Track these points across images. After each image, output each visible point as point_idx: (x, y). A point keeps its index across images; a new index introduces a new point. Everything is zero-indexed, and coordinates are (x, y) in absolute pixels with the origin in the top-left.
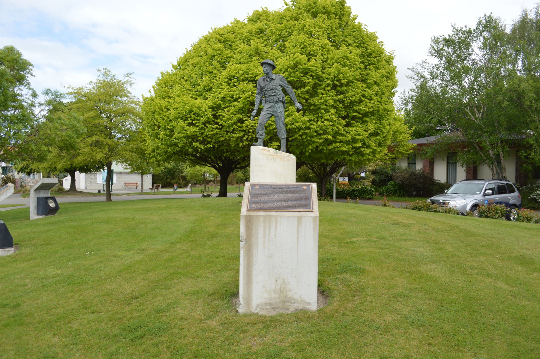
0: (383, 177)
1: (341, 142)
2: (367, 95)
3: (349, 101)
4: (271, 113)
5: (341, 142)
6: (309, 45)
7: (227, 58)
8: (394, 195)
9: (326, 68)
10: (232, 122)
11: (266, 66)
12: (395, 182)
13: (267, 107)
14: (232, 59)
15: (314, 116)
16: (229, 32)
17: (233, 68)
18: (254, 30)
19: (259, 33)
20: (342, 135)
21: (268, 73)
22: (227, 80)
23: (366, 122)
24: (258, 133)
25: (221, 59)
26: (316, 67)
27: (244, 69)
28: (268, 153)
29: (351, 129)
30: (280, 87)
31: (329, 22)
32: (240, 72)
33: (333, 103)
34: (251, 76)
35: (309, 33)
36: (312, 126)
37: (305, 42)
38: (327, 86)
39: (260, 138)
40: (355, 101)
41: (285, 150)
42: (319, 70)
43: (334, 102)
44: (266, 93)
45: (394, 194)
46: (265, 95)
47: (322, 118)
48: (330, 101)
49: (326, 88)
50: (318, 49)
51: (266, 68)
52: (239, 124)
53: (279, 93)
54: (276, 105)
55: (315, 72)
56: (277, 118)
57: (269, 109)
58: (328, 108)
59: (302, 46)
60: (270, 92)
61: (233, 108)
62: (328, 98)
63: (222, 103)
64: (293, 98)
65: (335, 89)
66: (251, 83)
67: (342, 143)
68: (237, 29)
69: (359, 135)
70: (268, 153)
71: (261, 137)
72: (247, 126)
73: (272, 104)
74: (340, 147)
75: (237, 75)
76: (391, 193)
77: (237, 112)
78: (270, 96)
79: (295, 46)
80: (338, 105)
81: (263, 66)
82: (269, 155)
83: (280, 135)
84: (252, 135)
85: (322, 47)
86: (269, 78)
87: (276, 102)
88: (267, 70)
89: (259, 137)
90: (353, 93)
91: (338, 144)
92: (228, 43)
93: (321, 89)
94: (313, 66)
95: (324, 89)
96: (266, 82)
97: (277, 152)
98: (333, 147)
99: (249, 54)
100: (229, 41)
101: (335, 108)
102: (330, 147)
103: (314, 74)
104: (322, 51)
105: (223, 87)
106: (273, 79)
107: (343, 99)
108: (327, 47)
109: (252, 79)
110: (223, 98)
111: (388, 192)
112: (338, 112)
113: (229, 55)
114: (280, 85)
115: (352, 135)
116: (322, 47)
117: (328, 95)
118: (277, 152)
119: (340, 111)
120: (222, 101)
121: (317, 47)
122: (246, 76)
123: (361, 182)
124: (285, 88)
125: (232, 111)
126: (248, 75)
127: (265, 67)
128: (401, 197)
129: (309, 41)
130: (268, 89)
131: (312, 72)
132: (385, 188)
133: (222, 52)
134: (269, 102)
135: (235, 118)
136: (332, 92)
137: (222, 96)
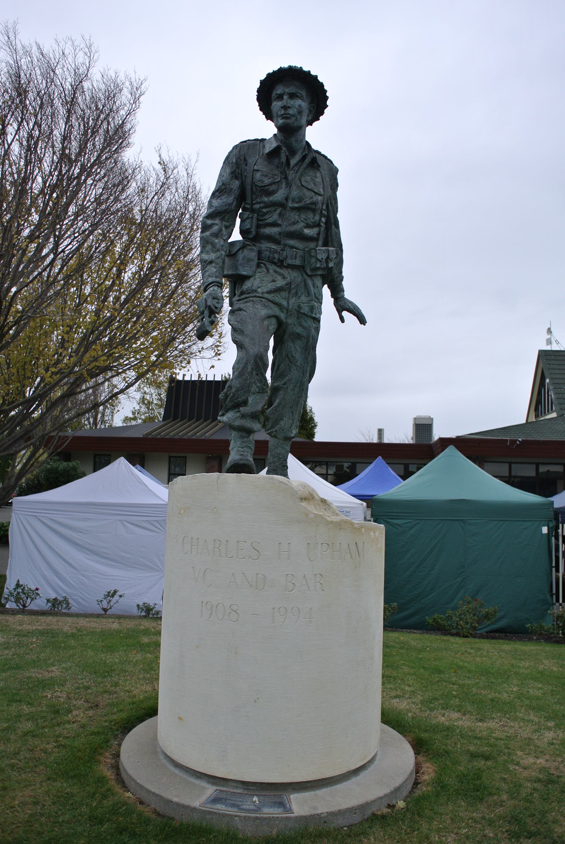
4: (282, 316)
13: (271, 286)
24: (245, 403)
51: (298, 102)
57: (277, 298)
60: (294, 216)
78: (292, 235)
130: (290, 204)
134: (280, 264)
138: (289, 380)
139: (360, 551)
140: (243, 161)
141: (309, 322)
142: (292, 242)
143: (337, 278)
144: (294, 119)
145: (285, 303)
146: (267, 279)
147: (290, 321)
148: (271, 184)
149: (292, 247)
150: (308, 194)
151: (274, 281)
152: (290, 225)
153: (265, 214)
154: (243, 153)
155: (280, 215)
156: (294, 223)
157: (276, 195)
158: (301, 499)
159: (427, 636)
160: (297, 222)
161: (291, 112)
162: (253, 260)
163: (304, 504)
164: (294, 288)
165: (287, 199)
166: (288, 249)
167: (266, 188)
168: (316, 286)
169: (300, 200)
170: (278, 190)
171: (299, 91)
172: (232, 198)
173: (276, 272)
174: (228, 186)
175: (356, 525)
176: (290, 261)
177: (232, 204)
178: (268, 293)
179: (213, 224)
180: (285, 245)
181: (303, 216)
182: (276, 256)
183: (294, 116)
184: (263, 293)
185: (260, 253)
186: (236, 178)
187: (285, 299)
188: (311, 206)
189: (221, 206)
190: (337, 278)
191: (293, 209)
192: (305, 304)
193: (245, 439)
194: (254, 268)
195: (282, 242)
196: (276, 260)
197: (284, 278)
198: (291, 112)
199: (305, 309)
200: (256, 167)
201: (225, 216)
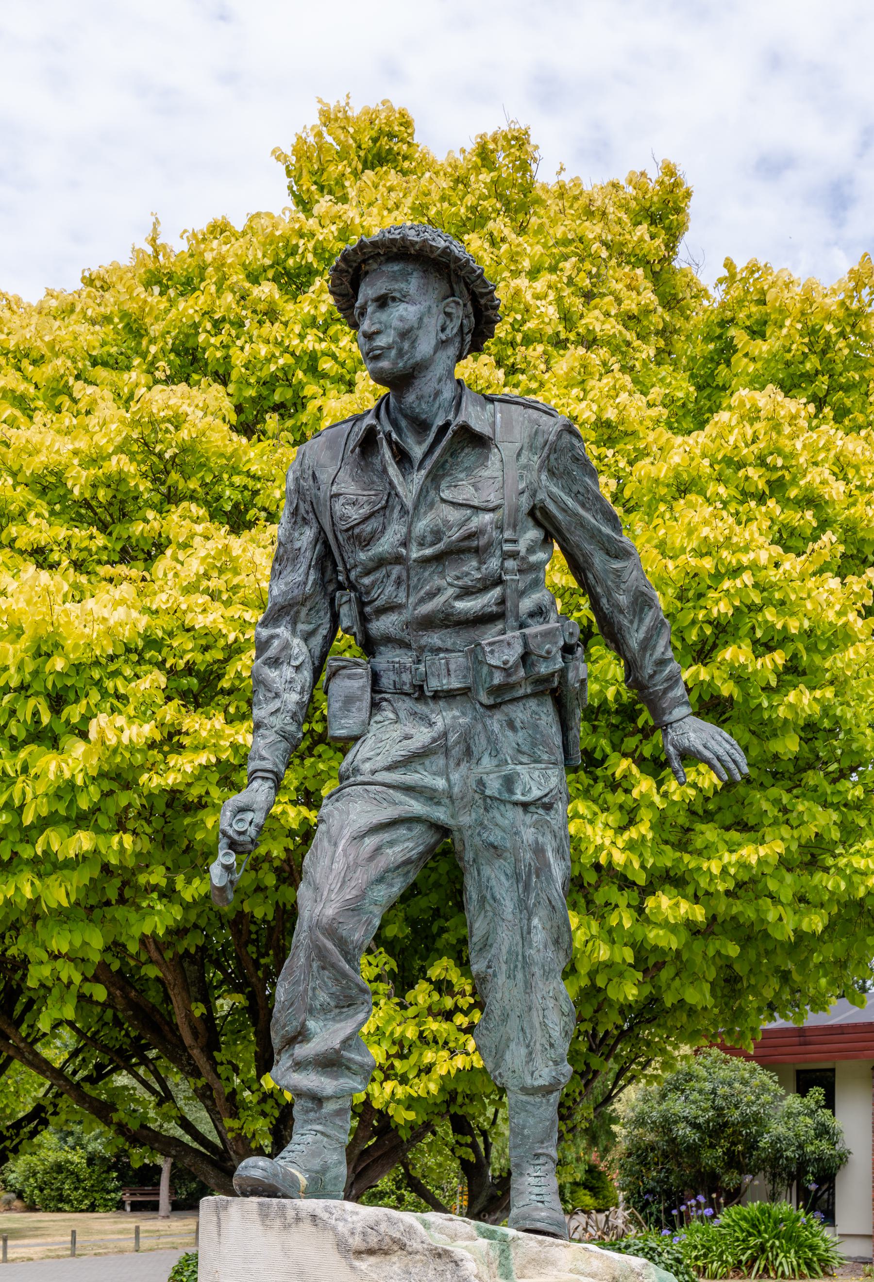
4: (440, 814)
13: (398, 752)
78: (428, 623)
89: (310, 1080)
96: (393, 471)
127: (383, 302)
130: (415, 554)
140: (311, 482)
142: (435, 639)
143: (651, 677)
144: (393, 352)
145: (440, 783)
146: (395, 734)
147: (465, 819)
148: (366, 519)
150: (454, 515)
151: (408, 737)
152: (422, 601)
157: (382, 540)
161: (381, 341)
164: (457, 743)
165: (405, 544)
167: (357, 531)
169: (437, 535)
170: (384, 528)
174: (289, 546)
176: (434, 684)
177: (305, 583)
178: (389, 768)
180: (422, 649)
183: (389, 348)
184: (374, 772)
188: (466, 544)
189: (284, 594)
191: (425, 561)
192: (492, 776)
194: (365, 714)
196: (407, 688)
197: (431, 724)
200: (335, 489)
201: (298, 612)
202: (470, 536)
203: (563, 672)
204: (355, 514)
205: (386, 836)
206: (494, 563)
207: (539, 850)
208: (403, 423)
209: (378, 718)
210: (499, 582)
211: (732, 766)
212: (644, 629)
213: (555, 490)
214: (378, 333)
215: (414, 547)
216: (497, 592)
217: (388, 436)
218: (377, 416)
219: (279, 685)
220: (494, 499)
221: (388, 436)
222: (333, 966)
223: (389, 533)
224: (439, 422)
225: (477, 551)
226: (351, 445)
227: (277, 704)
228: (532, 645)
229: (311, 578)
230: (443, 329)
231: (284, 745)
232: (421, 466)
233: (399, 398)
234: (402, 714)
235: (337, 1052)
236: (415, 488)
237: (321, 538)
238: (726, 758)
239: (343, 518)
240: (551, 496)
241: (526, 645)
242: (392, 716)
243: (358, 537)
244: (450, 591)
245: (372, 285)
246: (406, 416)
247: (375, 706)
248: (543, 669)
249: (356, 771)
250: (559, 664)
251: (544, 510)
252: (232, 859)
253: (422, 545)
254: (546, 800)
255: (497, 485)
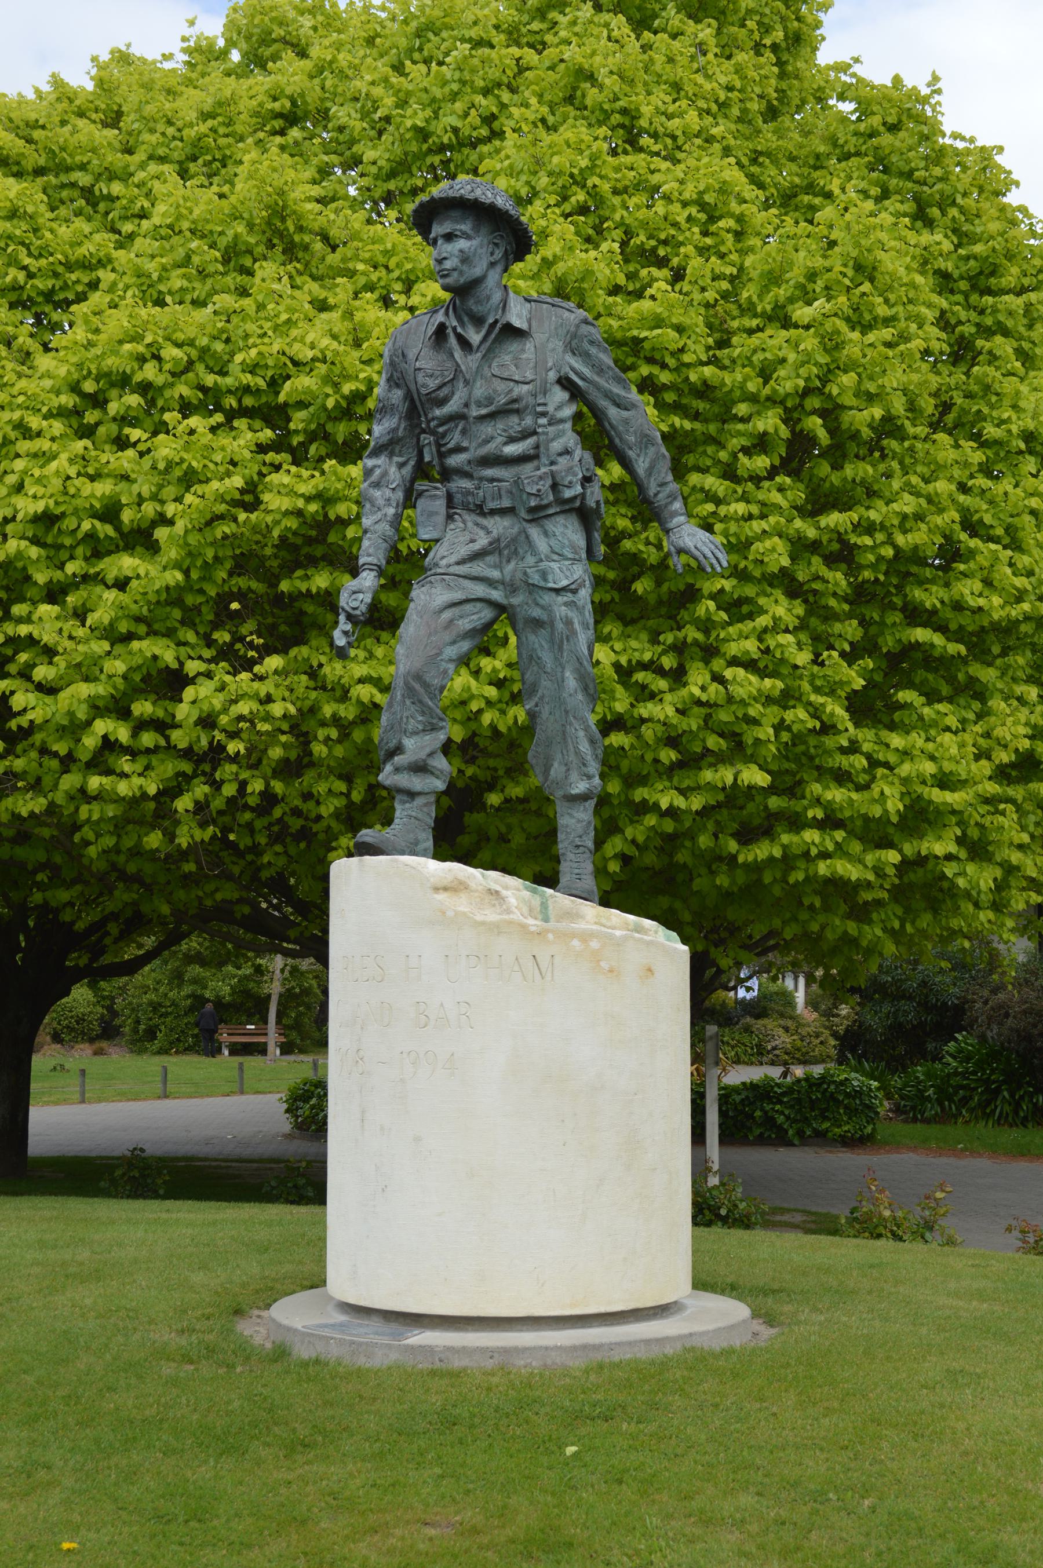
0: (910, 1013)
1: (830, 822)
2: (988, 519)
3: (888, 552)
4: (496, 595)
5: (830, 822)
6: (616, 192)
7: (69, 267)
8: (984, 1112)
9: (731, 333)
10: (100, 689)
11: (466, 227)
12: (982, 1038)
13: (464, 551)
14: (106, 276)
15: (654, 641)
16: (81, 114)
17: (117, 322)
18: (246, 105)
19: (278, 124)
20: (842, 777)
21: (477, 282)
22: (67, 400)
23: (978, 693)
24: (399, 750)
25: (31, 276)
26: (680, 329)
27: (191, 332)
28: (491, 915)
29: (897, 741)
30: (560, 395)
31: (728, 65)
32: (170, 352)
33: (785, 562)
34: (247, 379)
35: (616, 119)
36: (646, 710)
37: (591, 169)
38: (746, 451)
39: (412, 795)
40: (916, 557)
41: (589, 882)
42: (697, 350)
43: (793, 559)
44: (455, 439)
45: (984, 1105)
46: (442, 456)
47: (709, 652)
48: (768, 544)
49: (743, 459)
50: (681, 219)
51: (462, 244)
52: (143, 708)
53: (556, 446)
54: (534, 532)
55: (671, 362)
56: (538, 641)
57: (477, 568)
58: (750, 591)
59: (580, 196)
60: (487, 429)
61: (111, 595)
62: (757, 526)
63: (34, 552)
64: (652, 489)
65: (795, 474)
66: (241, 423)
67: (839, 835)
68: (130, 99)
69: (944, 782)
70: (491, 915)
71: (417, 783)
72: (207, 722)
73: (499, 526)
74: (825, 855)
75: (150, 372)
76: (964, 1101)
77: (138, 619)
78: (487, 461)
79: (530, 202)
80: (817, 578)
81: (438, 229)
82: (496, 929)
83: (557, 770)
84: (244, 775)
85: (703, 206)
86: (478, 321)
87: (537, 514)
88: (465, 259)
89: (404, 780)
90: (908, 504)
91: (811, 835)
92: (73, 185)
93: (704, 471)
94: (658, 322)
95: (730, 474)
96: (458, 354)
97: (544, 906)
98: (777, 853)
99: (223, 242)
100: (83, 167)
101: (794, 590)
102: (762, 851)
103: (665, 377)
104: (705, 233)
105: (44, 444)
106: (511, 332)
107: (853, 539)
108: (735, 207)
109: (248, 401)
110: (47, 520)
111: (951, 1101)
112: (814, 622)
113: (86, 249)
114: (565, 383)
115: (905, 781)
116: (703, 206)
117: (755, 509)
118: (544, 906)
119: (830, 616)
120: (35, 541)
121: (676, 207)
122: (210, 380)
123: (747, 1030)
124: (603, 403)
125: (100, 616)
126: (223, 373)
127: (449, 237)
128: (1024, 1122)
129: (617, 169)
130: (475, 412)
131: (650, 360)
132: (929, 1075)
133: (35, 231)
134: (480, 510)
135: (119, 667)
136: (781, 490)
137: (40, 507)
138: (542, 698)
139: (543, 970)
141: (546, 597)
142: (489, 472)
143: (656, 495)
147: (515, 601)
148: (440, 388)
149: (492, 480)
150: (501, 386)
151: (472, 541)
152: (480, 445)
153: (444, 435)
154: (399, 343)
155: (464, 432)
156: (487, 441)
158: (436, 889)
159: (849, 1155)
160: (492, 438)
161: (448, 265)
162: (437, 513)
163: (441, 896)
165: (466, 405)
166: (486, 485)
168: (550, 533)
169: (490, 400)
170: (453, 393)
171: (458, 227)
172: (395, 420)
173: (477, 524)
175: (533, 929)
176: (492, 505)
178: (458, 563)
179: (375, 466)
180: (481, 479)
181: (500, 425)
182: (470, 499)
183: (454, 270)
185: (450, 497)
186: (398, 386)
187: (495, 567)
190: (656, 495)
191: (482, 418)
193: (407, 805)
195: (475, 475)
197: (488, 533)
198: (448, 265)
199: (535, 579)
202: (515, 401)
203: (583, 496)
204: (432, 384)
205: (456, 611)
206: (528, 421)
207: (569, 622)
208: (466, 319)
209: (452, 526)
210: (535, 433)
211: (714, 561)
212: (648, 460)
213: (576, 365)
214: (445, 258)
215: (473, 407)
216: (531, 441)
217: (454, 329)
218: (447, 314)
219: (381, 502)
220: (529, 375)
221: (454, 329)
222: (420, 702)
223: (456, 397)
224: (491, 321)
225: (517, 411)
226: (430, 332)
227: (379, 515)
228: (558, 479)
229: (403, 426)
230: (492, 254)
231: (385, 545)
232: (477, 350)
233: (462, 302)
234: (470, 524)
235: (424, 761)
236: (474, 366)
237: (409, 396)
238: (710, 555)
239: (424, 386)
240: (573, 369)
241: (553, 477)
242: (462, 525)
243: (436, 398)
244: (500, 439)
245: (441, 224)
246: (467, 314)
247: (450, 517)
248: (568, 494)
249: (436, 565)
250: (579, 489)
251: (568, 379)
252: (349, 627)
253: (479, 404)
254: (573, 587)
255: (532, 365)
